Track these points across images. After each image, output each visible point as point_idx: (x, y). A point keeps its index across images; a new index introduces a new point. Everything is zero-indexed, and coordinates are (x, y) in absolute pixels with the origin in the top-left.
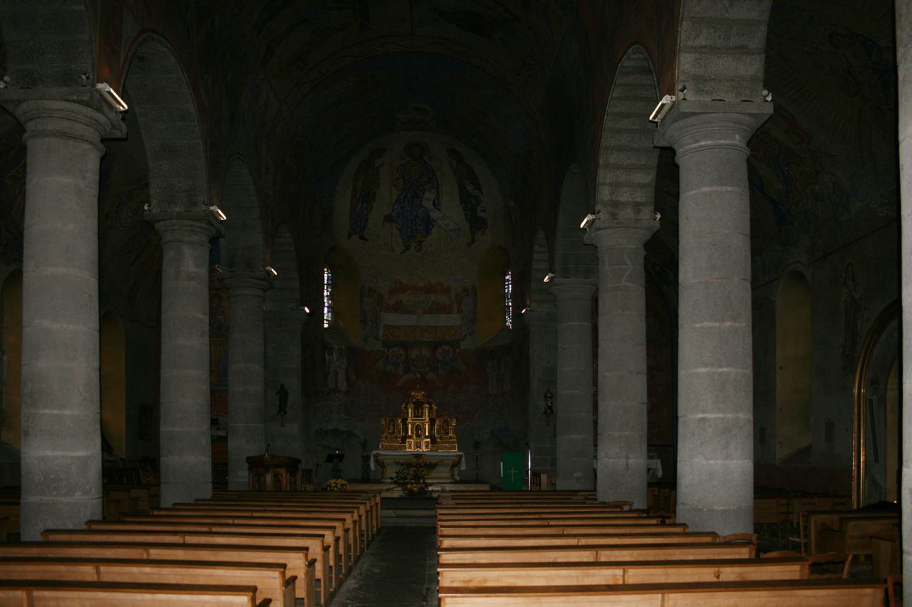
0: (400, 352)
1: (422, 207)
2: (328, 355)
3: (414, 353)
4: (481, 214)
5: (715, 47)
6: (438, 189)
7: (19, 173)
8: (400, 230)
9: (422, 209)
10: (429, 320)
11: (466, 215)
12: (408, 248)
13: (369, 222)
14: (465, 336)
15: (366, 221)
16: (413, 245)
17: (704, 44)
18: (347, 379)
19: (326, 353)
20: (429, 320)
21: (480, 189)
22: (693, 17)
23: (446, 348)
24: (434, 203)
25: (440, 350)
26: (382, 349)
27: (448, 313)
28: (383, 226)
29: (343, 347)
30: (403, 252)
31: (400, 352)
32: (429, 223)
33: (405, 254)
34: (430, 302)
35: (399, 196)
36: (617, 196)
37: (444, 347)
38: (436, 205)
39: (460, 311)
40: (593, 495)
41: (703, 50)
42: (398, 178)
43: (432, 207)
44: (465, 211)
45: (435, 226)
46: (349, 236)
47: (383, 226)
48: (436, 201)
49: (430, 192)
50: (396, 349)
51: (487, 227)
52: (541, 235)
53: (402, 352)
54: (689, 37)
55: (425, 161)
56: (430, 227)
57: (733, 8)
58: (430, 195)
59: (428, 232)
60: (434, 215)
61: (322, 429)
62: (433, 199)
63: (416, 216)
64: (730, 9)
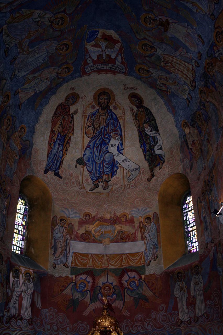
0: (88, 280)
1: (108, 152)
2: (14, 277)
3: (101, 281)
4: (158, 152)
6: (121, 136)
8: (90, 172)
10: (115, 248)
11: (145, 155)
12: (97, 186)
13: (64, 162)
14: (150, 261)
15: (62, 162)
16: (101, 184)
18: (33, 305)
20: (115, 248)
21: (157, 130)
23: (132, 274)
24: (118, 149)
25: (126, 278)
29: (32, 271)
30: (92, 190)
31: (88, 280)
32: (114, 165)
33: (95, 191)
34: (116, 232)
35: (90, 142)
36: (219, 267)
37: (129, 273)
38: (120, 150)
39: (143, 238)
42: (89, 127)
44: (143, 152)
45: (119, 168)
46: (46, 171)
47: (76, 167)
48: (120, 147)
50: (84, 277)
51: (164, 162)
52: (166, 307)
53: (89, 279)
55: (111, 110)
56: (115, 169)
58: (114, 142)
59: (113, 173)
60: (119, 158)
62: (117, 145)
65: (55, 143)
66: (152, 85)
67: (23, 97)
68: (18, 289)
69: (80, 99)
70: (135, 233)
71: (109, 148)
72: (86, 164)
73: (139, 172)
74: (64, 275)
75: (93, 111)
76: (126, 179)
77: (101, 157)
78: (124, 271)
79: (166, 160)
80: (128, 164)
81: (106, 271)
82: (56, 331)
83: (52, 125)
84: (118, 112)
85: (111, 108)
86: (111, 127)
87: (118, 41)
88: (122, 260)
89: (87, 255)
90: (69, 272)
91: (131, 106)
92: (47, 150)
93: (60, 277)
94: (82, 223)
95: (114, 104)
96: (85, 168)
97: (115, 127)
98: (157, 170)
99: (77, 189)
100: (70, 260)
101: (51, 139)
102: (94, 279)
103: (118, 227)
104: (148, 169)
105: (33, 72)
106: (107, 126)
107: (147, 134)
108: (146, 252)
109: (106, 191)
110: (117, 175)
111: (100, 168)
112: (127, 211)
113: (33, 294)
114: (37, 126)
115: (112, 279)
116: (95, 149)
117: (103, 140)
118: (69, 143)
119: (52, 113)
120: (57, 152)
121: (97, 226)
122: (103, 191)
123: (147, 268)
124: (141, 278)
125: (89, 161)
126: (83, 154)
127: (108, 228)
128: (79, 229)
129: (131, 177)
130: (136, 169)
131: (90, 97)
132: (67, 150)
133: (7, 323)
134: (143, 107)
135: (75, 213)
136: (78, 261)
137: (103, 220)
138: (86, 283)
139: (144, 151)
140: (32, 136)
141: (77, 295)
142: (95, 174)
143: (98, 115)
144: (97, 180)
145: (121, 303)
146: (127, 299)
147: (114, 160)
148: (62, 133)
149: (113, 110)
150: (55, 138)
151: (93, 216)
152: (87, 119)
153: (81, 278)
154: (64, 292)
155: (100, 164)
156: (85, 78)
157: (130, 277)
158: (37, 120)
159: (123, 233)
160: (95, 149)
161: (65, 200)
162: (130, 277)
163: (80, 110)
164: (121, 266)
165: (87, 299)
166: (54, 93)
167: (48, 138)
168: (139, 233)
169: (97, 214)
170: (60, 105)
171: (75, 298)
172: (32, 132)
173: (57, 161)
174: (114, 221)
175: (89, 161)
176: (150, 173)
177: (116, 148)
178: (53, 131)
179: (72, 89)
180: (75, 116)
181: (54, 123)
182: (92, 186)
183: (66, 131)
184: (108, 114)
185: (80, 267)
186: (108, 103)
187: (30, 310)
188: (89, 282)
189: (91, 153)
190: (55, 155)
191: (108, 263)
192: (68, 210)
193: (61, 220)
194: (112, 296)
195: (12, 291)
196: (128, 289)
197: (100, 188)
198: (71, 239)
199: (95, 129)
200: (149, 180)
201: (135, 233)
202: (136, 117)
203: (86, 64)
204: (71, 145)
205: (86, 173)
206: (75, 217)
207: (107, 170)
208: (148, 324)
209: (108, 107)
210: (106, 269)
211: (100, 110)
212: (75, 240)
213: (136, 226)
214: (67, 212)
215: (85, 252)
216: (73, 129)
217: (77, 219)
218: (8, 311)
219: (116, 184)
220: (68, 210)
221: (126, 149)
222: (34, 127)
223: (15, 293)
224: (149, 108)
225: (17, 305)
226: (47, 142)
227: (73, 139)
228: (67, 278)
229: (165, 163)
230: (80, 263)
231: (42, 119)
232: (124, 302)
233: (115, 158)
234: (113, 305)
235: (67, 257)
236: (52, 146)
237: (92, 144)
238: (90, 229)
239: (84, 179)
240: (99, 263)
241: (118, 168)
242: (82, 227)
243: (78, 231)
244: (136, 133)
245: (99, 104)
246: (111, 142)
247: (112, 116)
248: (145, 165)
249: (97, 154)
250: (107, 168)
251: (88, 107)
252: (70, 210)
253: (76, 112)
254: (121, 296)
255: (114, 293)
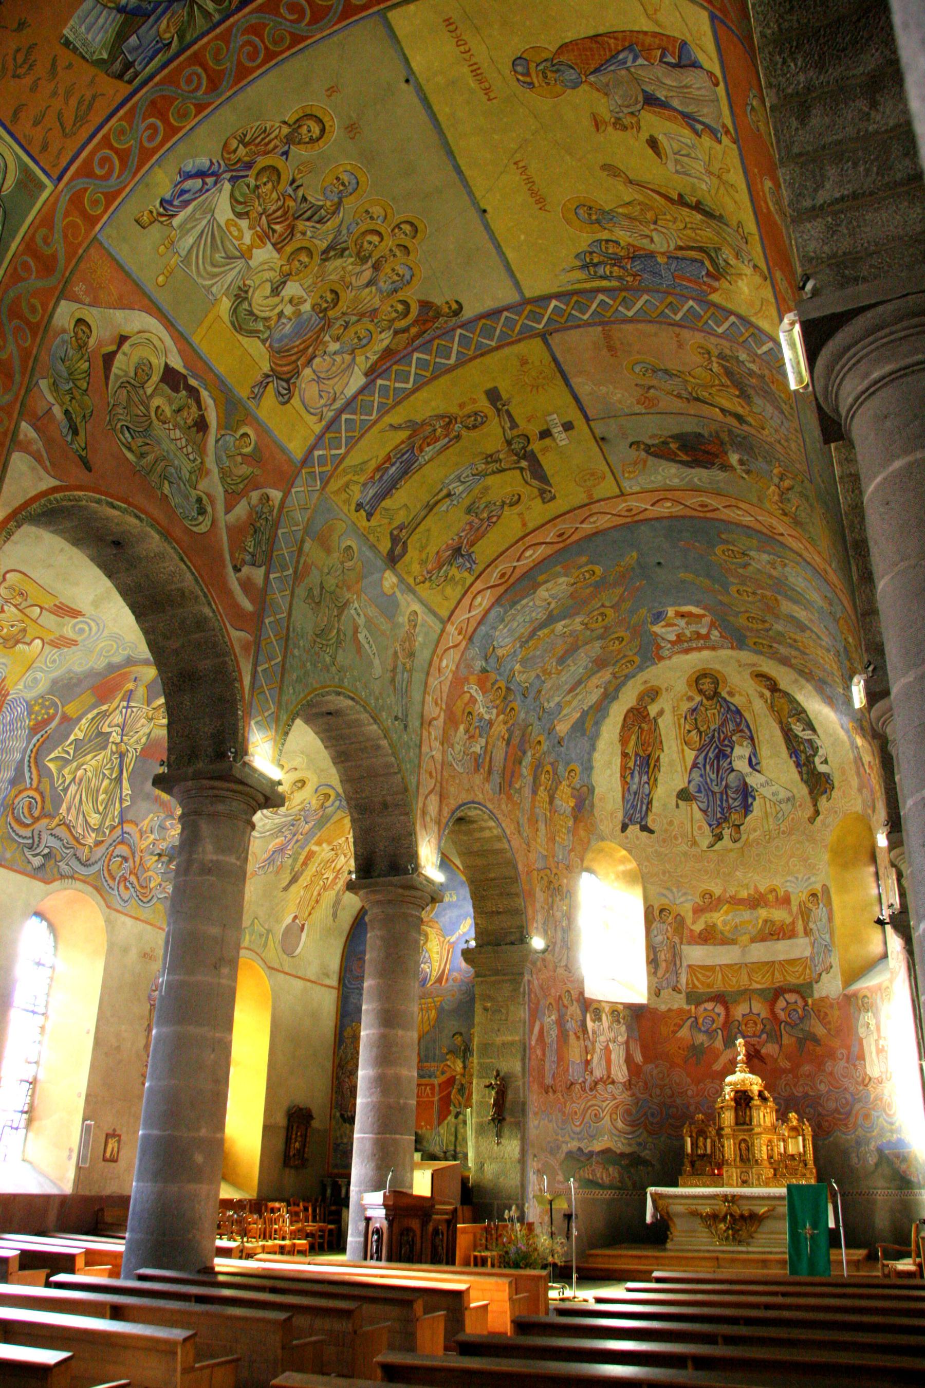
0: (717, 1010)
1: (733, 770)
2: (593, 1021)
3: (739, 1011)
4: (822, 768)
5: (864, 194)
6: (752, 739)
7: (68, 753)
8: (705, 812)
9: (733, 774)
10: (760, 952)
11: (800, 773)
12: (719, 837)
13: (655, 803)
15: (650, 803)
16: (726, 832)
17: (838, 195)
19: (588, 1016)
20: (760, 952)
21: (813, 730)
22: (800, 155)
23: (792, 997)
25: (781, 1003)
26: (686, 1007)
27: (790, 938)
28: (677, 806)
31: (717, 1010)
32: (746, 794)
33: (717, 847)
34: (760, 921)
35: (697, 757)
37: (787, 996)
39: (808, 932)
40: (379, 1250)
41: (837, 207)
42: (689, 731)
43: (749, 770)
47: (677, 806)
49: (741, 745)
50: (709, 1006)
53: (720, 1009)
54: (800, 194)
55: (724, 699)
56: (750, 800)
57: (881, 109)
58: (740, 753)
59: (747, 809)
60: (754, 780)
61: (580, 1149)
63: (727, 786)
64: (873, 114)
65: (632, 774)
66: (785, 661)
67: (562, 728)
68: (602, 1038)
69: (664, 693)
70: (793, 923)
71: (734, 764)
72: (695, 798)
73: (793, 805)
74: (675, 1007)
75: (692, 705)
76: (771, 820)
77: (722, 780)
78: (779, 992)
79: (836, 784)
80: (774, 788)
81: (746, 994)
82: (670, 1097)
83: (622, 745)
84: (737, 700)
85: (724, 694)
86: (731, 726)
87: (703, 616)
88: (773, 974)
89: (711, 968)
90: (684, 1001)
91: (759, 689)
92: (620, 788)
93: (670, 1010)
94: (698, 911)
95: (728, 689)
96: (695, 806)
97: (738, 725)
98: (823, 803)
99: (684, 848)
100: (683, 979)
101: (624, 768)
102: (727, 1009)
103: (763, 913)
104: (808, 799)
105: (572, 690)
106: (722, 725)
107: (796, 736)
108: (812, 959)
109: (738, 845)
110: (755, 813)
111: (721, 800)
112: (777, 882)
113: (627, 1043)
114: (596, 755)
115: (759, 1008)
116: (708, 767)
117: (720, 750)
118: (657, 766)
119: (619, 726)
120: (639, 788)
121: (726, 913)
122: (731, 845)
123: (815, 986)
124: (806, 1004)
125: (699, 791)
126: (686, 781)
127: (746, 915)
128: (694, 923)
129: (780, 815)
130: (788, 799)
131: (681, 686)
132: (656, 780)
133: (591, 1090)
134: (780, 690)
135: (685, 894)
136: (698, 979)
137: (735, 901)
138: (715, 1017)
139: (798, 765)
140: (589, 776)
141: (701, 1038)
142: (715, 814)
143: (703, 709)
144: (719, 824)
145: (776, 1047)
146: (786, 1040)
147: (745, 784)
148: (641, 753)
149: (728, 698)
150: (631, 764)
151: (717, 895)
152: (682, 720)
153: (705, 1009)
154: (679, 1034)
155: (721, 793)
156: (661, 665)
157: (788, 1003)
158: (593, 748)
159: (773, 923)
160: (708, 767)
161: (664, 873)
162: (788, 1003)
163: (668, 709)
164: (773, 983)
165: (719, 1043)
166: (615, 698)
167: (618, 770)
168: (800, 922)
169: (725, 890)
170: (631, 710)
171: (697, 1043)
172: (588, 768)
173: (642, 803)
174: (756, 902)
175: (699, 791)
176: (812, 809)
177: (747, 761)
178: (625, 755)
179: (645, 682)
180: (660, 721)
181: (624, 741)
182: (711, 839)
183: (650, 749)
184: (721, 706)
185: (701, 989)
186: (716, 689)
187: (625, 1068)
188: (719, 1015)
189: (701, 776)
190: (635, 794)
191: (750, 979)
192: (671, 891)
193: (661, 911)
194: (760, 1037)
195: (593, 1044)
196: (787, 1023)
197: (726, 842)
198: (681, 943)
199: (701, 733)
200: (812, 820)
201: (793, 923)
202: (772, 707)
203: (659, 647)
204: (662, 769)
205: (698, 815)
206: (687, 901)
207: (736, 804)
208: (821, 1082)
209: (716, 694)
210: (746, 990)
211: (705, 701)
212: (689, 943)
213: (795, 909)
214: (670, 896)
215: (709, 962)
216: (661, 742)
217: (689, 906)
218: (592, 1073)
219: (755, 830)
220: (671, 891)
221: (764, 763)
222: (590, 760)
223: (597, 1045)
224: (790, 692)
225: (604, 1063)
226: (619, 775)
227: (664, 759)
228: (680, 1011)
229: (836, 790)
230: (702, 983)
231: (601, 744)
232: (781, 1046)
233: (748, 780)
234: (763, 1051)
235: (677, 974)
236: (628, 779)
237: (701, 760)
238: (714, 920)
239: (695, 828)
240: (734, 980)
241: (754, 799)
242: (699, 917)
243: (693, 928)
244: (778, 734)
245: (700, 692)
246: (735, 750)
247: (729, 708)
248: (802, 791)
249: (714, 776)
250: (735, 799)
251: (681, 700)
252: (675, 890)
253: (661, 713)
254: (775, 1037)
255: (763, 1031)
